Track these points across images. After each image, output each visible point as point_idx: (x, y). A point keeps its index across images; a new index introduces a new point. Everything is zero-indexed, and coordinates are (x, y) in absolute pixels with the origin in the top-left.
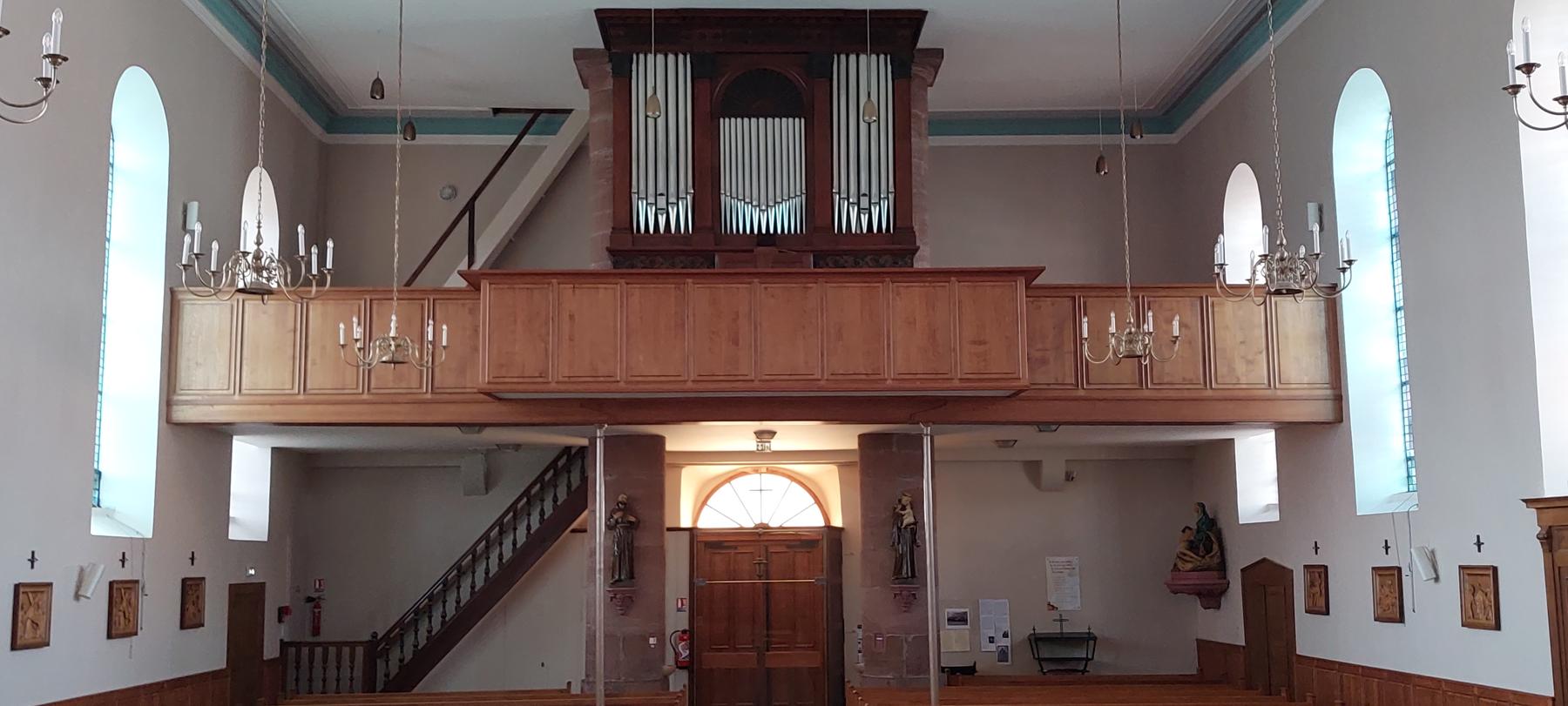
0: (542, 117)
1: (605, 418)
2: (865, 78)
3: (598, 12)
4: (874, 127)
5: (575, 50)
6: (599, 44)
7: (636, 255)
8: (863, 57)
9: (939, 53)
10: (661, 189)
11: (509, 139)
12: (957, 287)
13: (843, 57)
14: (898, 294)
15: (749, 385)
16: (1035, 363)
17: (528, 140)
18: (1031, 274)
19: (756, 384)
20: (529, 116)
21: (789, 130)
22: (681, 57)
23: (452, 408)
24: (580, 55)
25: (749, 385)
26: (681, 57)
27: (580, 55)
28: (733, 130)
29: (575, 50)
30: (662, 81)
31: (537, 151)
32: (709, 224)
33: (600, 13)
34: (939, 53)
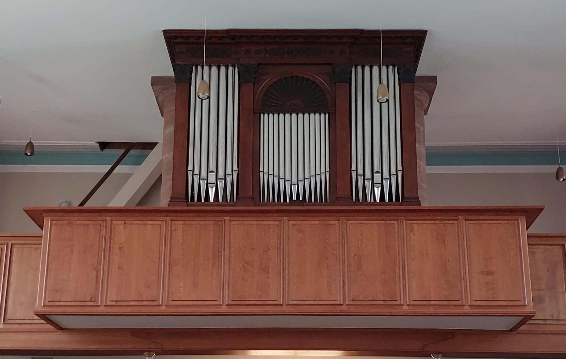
0: (132, 152)
1: (152, 346)
2: (376, 88)
3: (165, 32)
4: (385, 106)
5: (153, 78)
6: (171, 73)
7: (187, 204)
8: (376, 69)
9: (434, 80)
10: (212, 167)
11: (106, 168)
12: (469, 226)
13: (359, 68)
14: (412, 230)
15: (278, 309)
16: (538, 300)
17: (120, 169)
18: (531, 214)
19: (285, 308)
20: (121, 152)
21: (316, 124)
22: (231, 69)
23: (22, 337)
24: (156, 82)
25: (278, 309)
26: (231, 69)
27: (156, 82)
28: (270, 123)
29: (153, 78)
30: (217, 90)
31: (128, 176)
32: (250, 194)
33: (167, 33)
34: (434, 80)
